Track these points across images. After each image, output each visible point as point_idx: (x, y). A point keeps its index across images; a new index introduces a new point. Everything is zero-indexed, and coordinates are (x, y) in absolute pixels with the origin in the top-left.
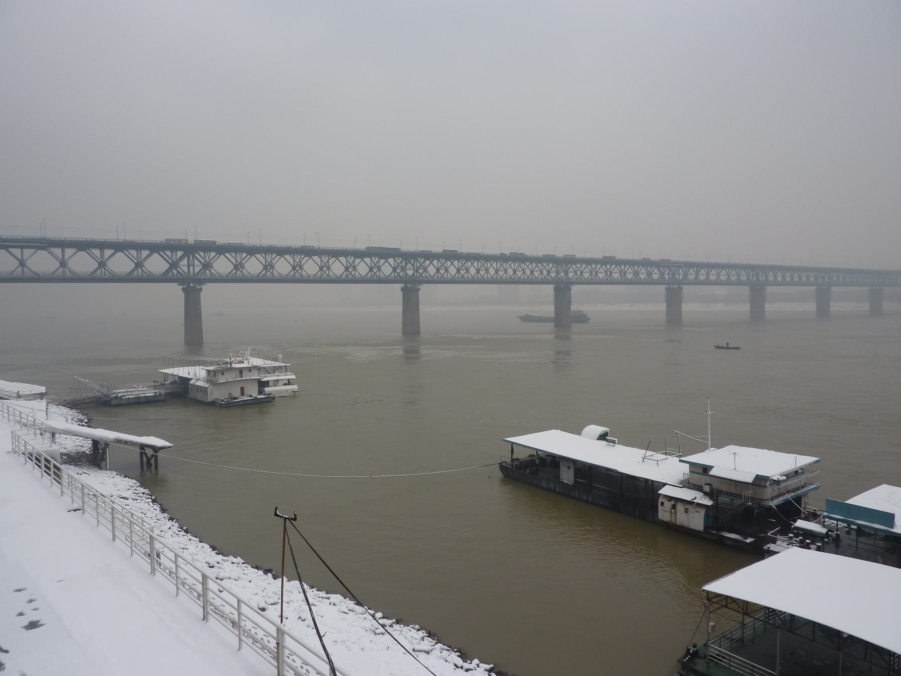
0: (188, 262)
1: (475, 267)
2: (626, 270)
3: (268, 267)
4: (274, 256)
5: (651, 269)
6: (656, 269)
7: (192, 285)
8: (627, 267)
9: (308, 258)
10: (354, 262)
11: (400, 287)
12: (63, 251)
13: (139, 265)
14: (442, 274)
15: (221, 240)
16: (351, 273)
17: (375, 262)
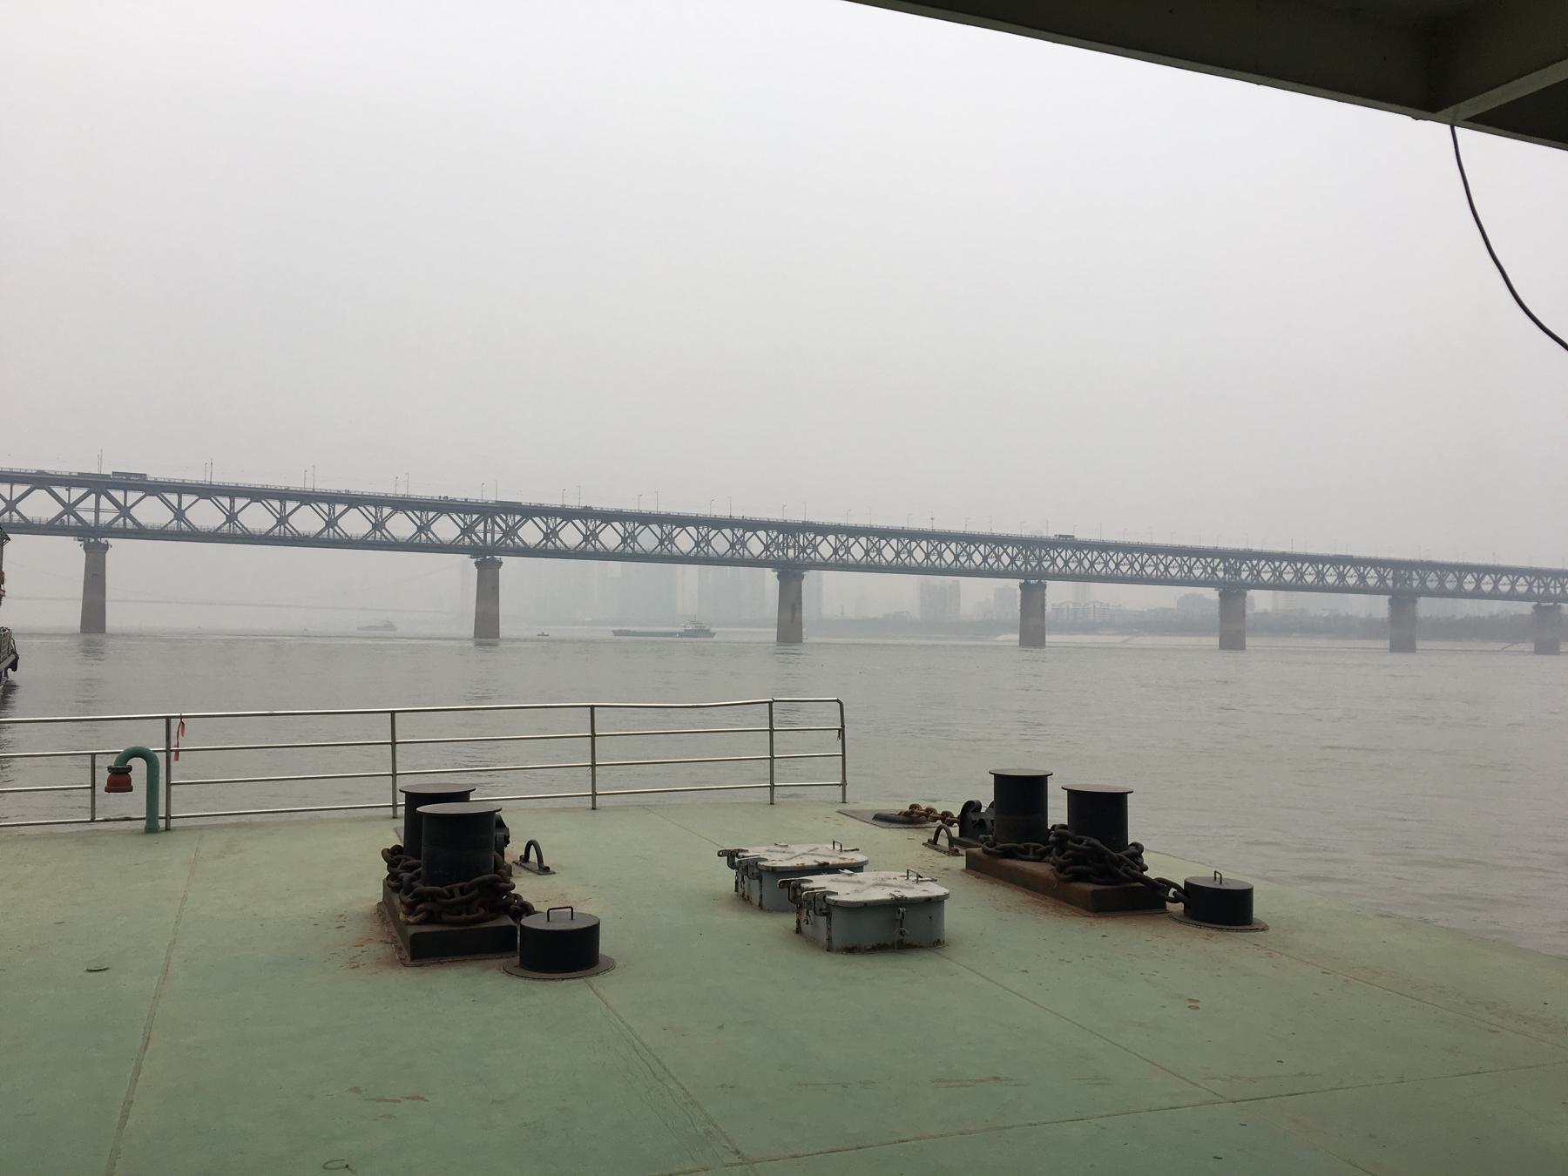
0: (485, 527)
2: (1282, 568)
3: (550, 535)
4: (559, 520)
5: (1384, 571)
6: (1352, 569)
7: (92, 540)
8: (1328, 566)
9: (643, 527)
10: (743, 536)
12: (180, 498)
13: (331, 523)
15: (526, 499)
16: (666, 547)
17: (773, 537)
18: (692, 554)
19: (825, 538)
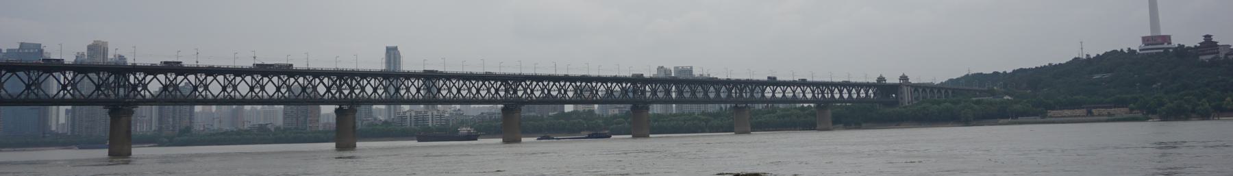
1: (274, 84)
5: (682, 87)
11: (334, 109)
14: (380, 94)
17: (140, 79)
18: (23, 96)
19: (215, 78)
